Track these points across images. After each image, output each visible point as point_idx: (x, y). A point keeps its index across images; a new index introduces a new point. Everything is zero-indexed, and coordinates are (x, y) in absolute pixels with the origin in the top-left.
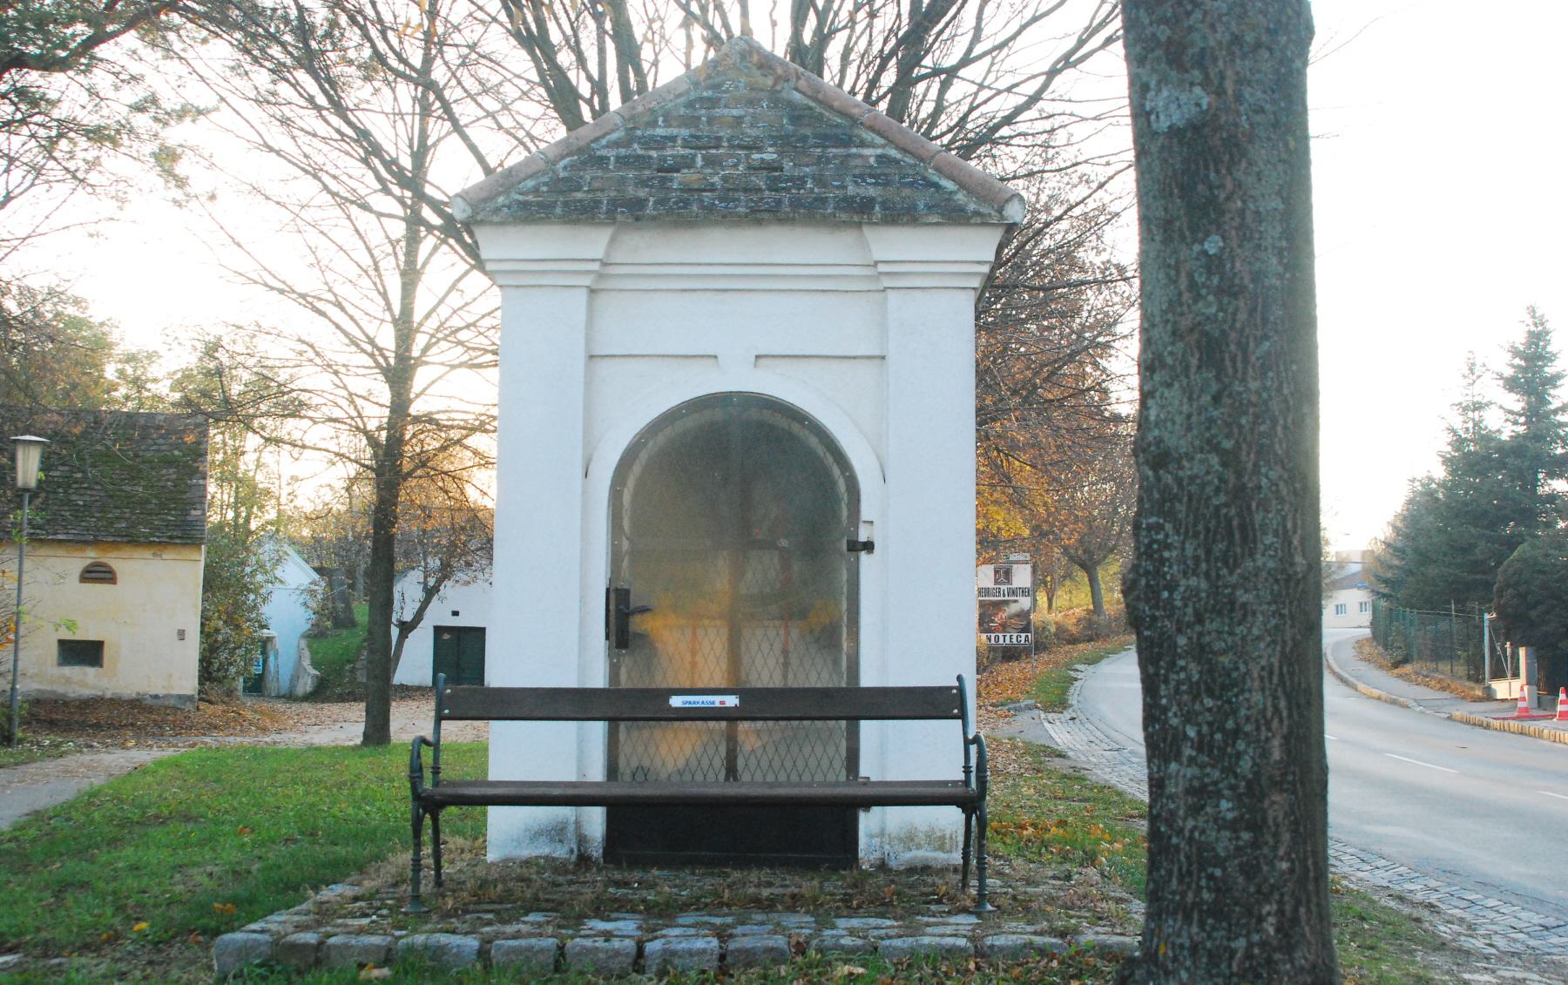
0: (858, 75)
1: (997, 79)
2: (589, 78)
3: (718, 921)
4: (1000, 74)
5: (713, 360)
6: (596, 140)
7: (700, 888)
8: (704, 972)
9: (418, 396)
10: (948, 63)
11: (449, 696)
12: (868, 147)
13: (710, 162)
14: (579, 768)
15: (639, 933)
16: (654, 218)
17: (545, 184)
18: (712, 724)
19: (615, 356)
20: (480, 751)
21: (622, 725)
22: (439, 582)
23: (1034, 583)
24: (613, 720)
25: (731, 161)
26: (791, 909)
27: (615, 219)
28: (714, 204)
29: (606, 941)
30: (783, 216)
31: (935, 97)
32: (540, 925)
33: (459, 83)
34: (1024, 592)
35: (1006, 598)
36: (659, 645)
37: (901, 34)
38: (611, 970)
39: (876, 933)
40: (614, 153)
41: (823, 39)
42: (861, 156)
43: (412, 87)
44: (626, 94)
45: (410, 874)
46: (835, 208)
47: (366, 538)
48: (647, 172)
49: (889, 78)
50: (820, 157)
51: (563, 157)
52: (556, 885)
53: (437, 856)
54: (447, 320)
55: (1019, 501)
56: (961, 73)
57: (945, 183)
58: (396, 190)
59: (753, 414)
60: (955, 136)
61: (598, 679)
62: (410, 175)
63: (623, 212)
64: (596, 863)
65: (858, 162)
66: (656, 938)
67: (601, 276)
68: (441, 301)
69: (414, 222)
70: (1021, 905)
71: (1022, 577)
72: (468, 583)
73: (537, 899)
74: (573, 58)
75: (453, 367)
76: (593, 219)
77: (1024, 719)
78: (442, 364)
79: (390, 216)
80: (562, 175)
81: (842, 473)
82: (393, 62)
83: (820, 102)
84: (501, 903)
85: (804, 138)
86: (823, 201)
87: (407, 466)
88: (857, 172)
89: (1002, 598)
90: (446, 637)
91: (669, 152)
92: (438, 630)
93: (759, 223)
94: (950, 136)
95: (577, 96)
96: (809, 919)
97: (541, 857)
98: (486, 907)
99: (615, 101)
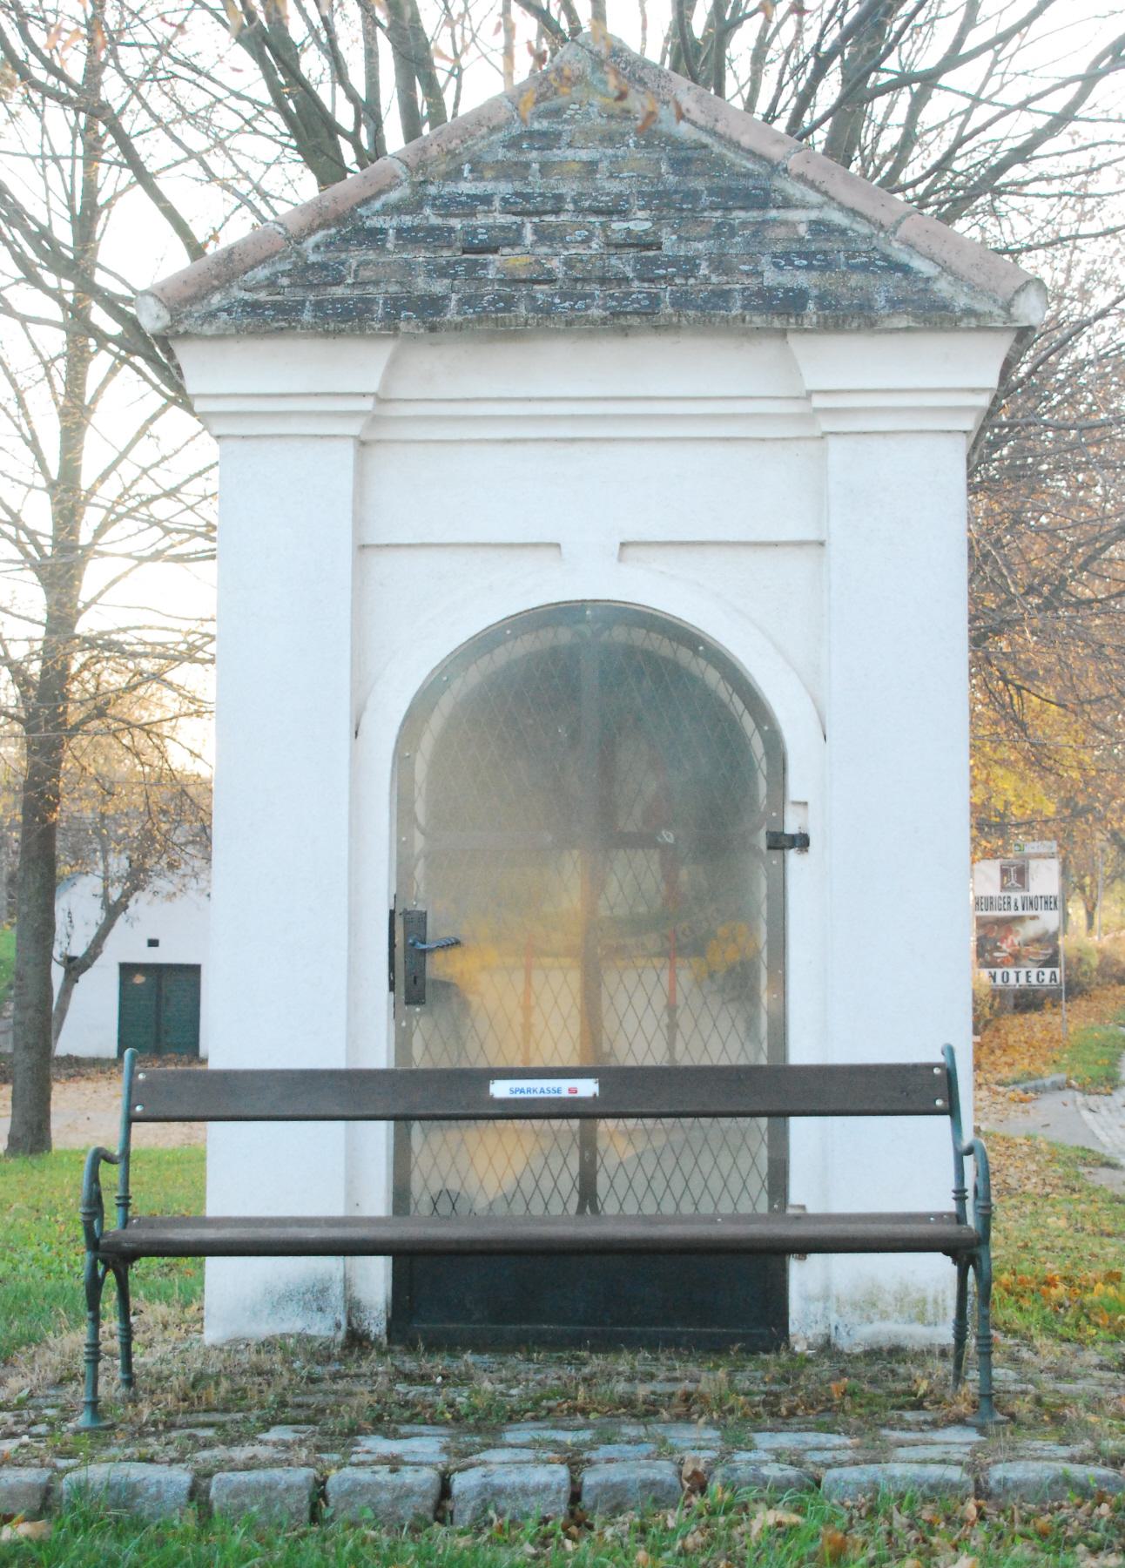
0: (780, 88)
1: (1002, 86)
2: (352, 96)
3: (568, 1438)
4: (1007, 78)
5: (553, 552)
6: (366, 201)
7: (539, 1383)
8: (545, 1521)
9: (87, 606)
10: (927, 61)
11: (146, 1083)
12: (796, 207)
13: (543, 235)
14: (349, 1195)
15: (444, 1458)
16: (458, 327)
17: (283, 273)
18: (556, 1123)
19: (398, 546)
20: (196, 1161)
21: (416, 1126)
22: (127, 895)
23: (1065, 889)
24: (402, 1119)
25: (581, 234)
26: (685, 1418)
27: (397, 329)
28: (553, 304)
29: (393, 1471)
30: (662, 321)
31: (902, 120)
32: (287, 1446)
33: (145, 106)
34: (1049, 903)
35: (1020, 913)
36: (474, 1000)
37: (848, 19)
38: (400, 1518)
39: (818, 1457)
40: (394, 223)
41: (723, 29)
42: (785, 223)
43: (71, 114)
44: (412, 132)
45: (82, 1366)
46: (744, 307)
47: (10, 828)
48: (446, 253)
49: (830, 91)
50: (719, 226)
51: (312, 231)
52: (312, 1380)
53: (127, 1333)
54: (134, 482)
55: (1040, 760)
56: (944, 80)
57: (918, 264)
58: (50, 279)
59: (619, 634)
60: (934, 183)
61: (378, 1055)
62: (71, 256)
63: (408, 318)
64: (375, 1344)
65: (781, 232)
66: (472, 1466)
67: (375, 419)
68: (123, 455)
69: (79, 327)
70: (1048, 1411)
71: (1045, 878)
72: (171, 896)
73: (283, 1404)
74: (326, 64)
75: (141, 560)
76: (362, 329)
77: (1049, 1106)
78: (129, 556)
79: (38, 321)
80: (313, 258)
81: (759, 727)
82: (40, 74)
83: (719, 137)
84: (226, 1410)
85: (694, 196)
86: (722, 296)
87: (74, 714)
88: (779, 248)
89: (1012, 913)
90: (139, 979)
91: (480, 220)
92: (127, 970)
93: (625, 331)
94: (927, 182)
95: (333, 129)
96: (712, 1434)
97: (291, 1336)
98: (203, 1418)
99: (394, 138)
